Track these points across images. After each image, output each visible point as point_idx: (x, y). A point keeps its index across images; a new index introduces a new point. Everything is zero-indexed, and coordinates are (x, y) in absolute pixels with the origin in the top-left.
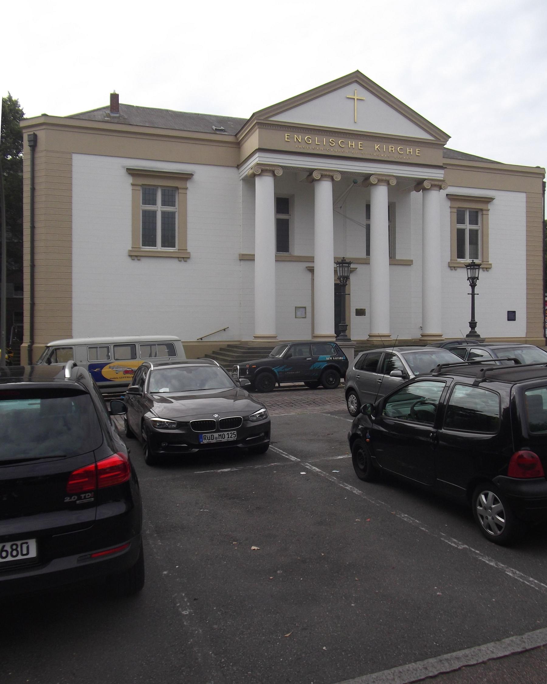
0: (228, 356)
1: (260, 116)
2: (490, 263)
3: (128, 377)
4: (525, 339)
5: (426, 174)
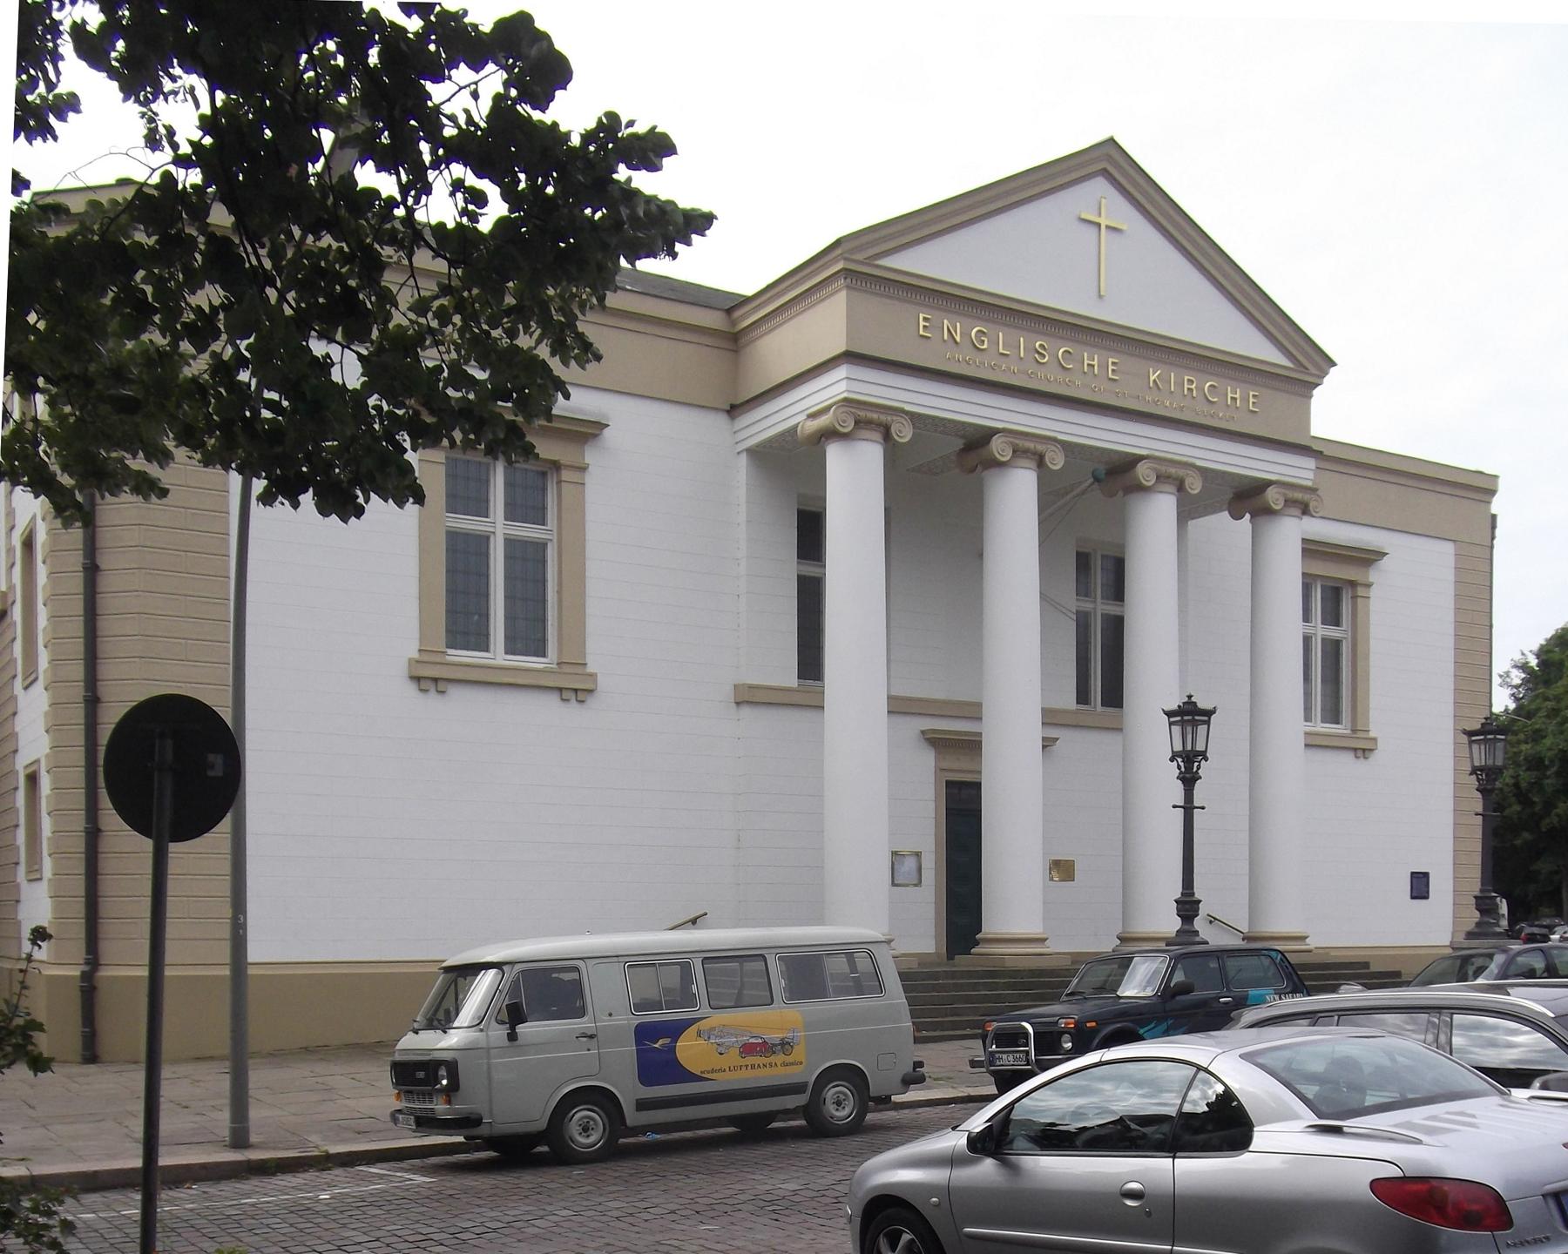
0: (986, 999)
1: (852, 251)
2: (1372, 734)
3: (753, 1067)
5: (1222, 458)
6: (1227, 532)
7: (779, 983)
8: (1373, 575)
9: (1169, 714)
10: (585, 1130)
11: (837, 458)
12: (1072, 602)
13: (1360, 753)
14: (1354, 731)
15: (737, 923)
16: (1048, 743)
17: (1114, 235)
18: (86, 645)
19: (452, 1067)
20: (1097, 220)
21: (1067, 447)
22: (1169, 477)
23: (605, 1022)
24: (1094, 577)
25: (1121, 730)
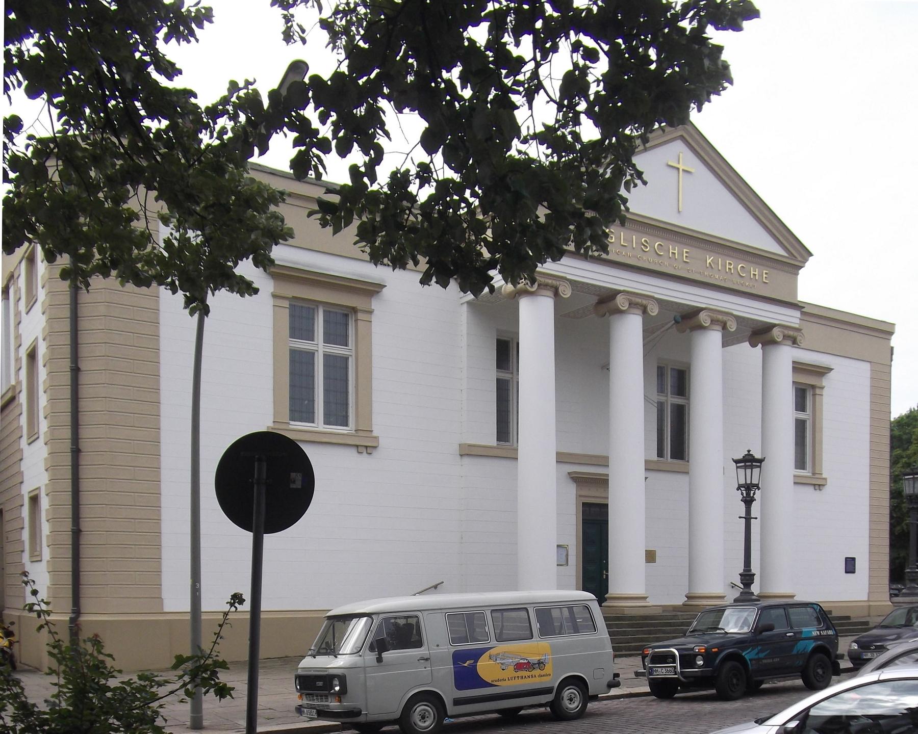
2: (824, 476)
3: (522, 677)
4: (867, 604)
6: (749, 354)
7: (536, 626)
8: (825, 382)
9: (737, 462)
10: (423, 717)
12: (655, 397)
13: (817, 487)
14: (814, 474)
15: (462, 590)
16: (646, 478)
17: (687, 176)
18: (72, 416)
19: (342, 679)
21: (660, 302)
22: (718, 321)
23: (435, 651)
24: (673, 383)
25: (687, 473)
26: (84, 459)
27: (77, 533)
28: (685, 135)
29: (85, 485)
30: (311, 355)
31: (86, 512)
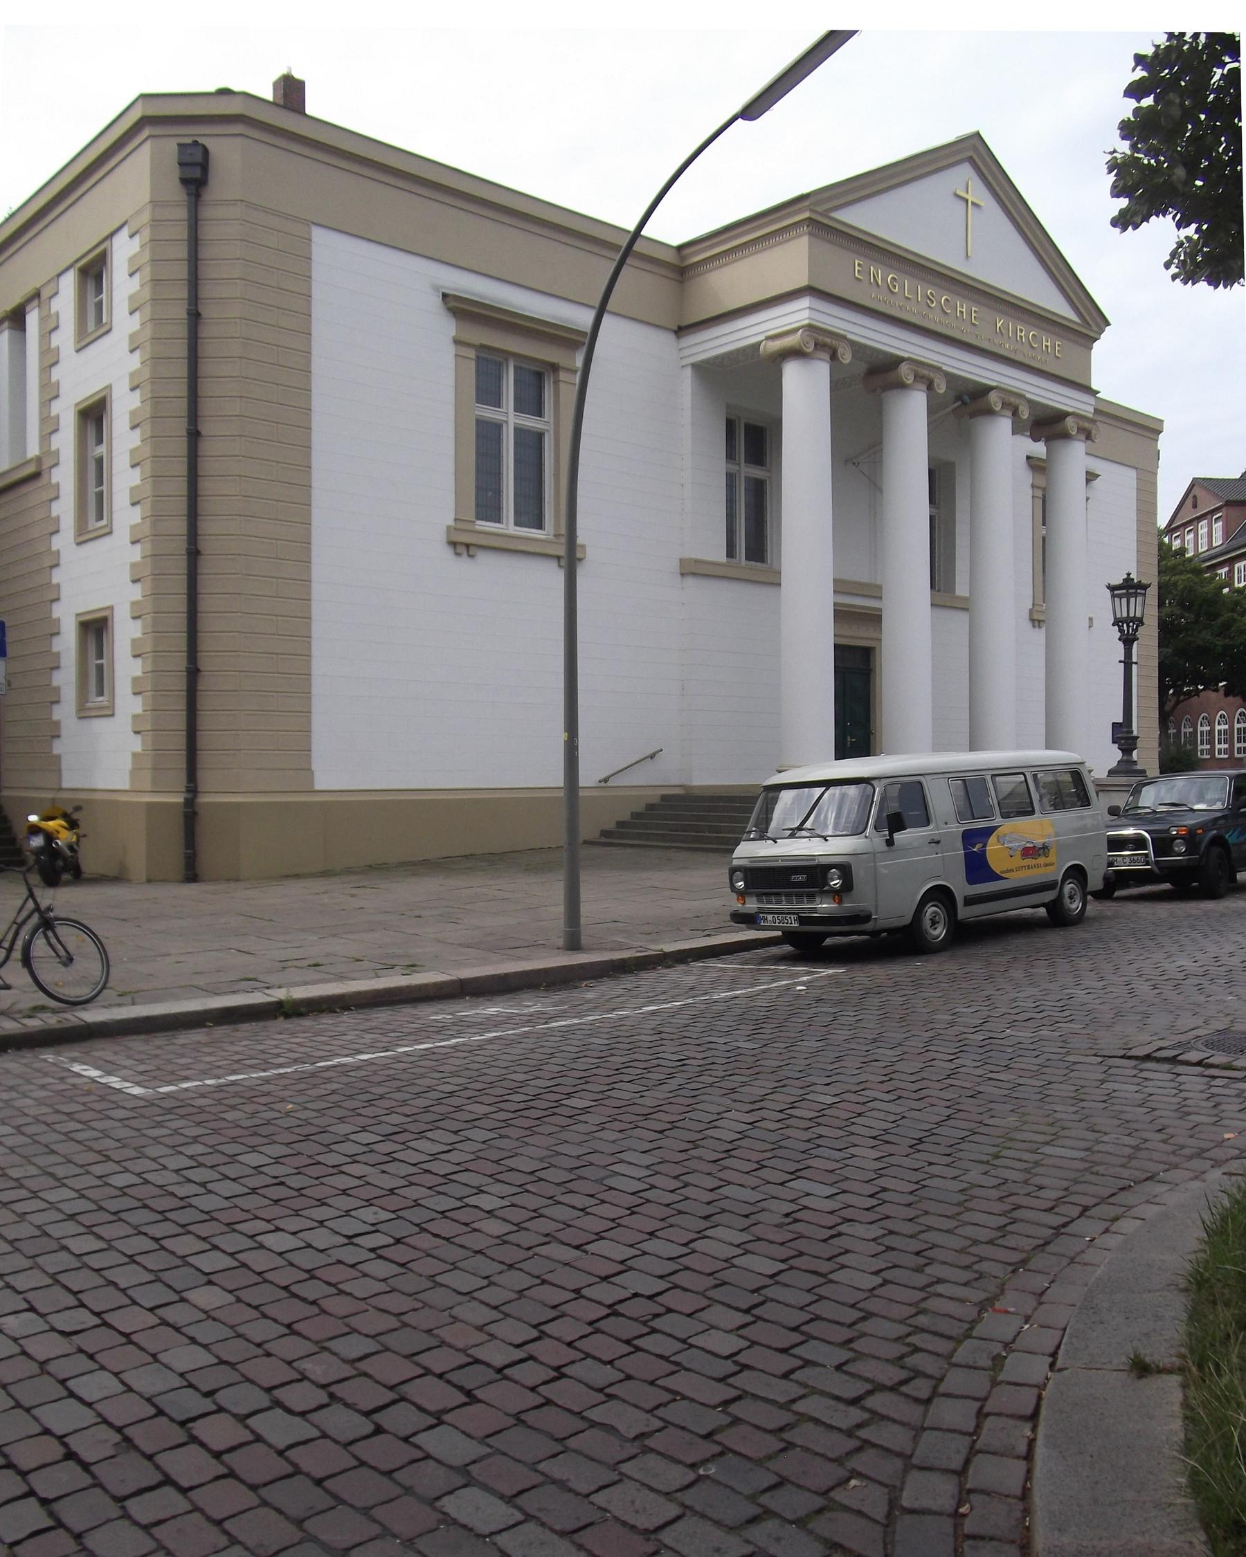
5: (1043, 393)
9: (1112, 588)
11: (792, 373)
19: (845, 870)
20: (963, 194)
25: (967, 610)
26: (207, 566)
27: (193, 673)
28: (975, 157)
29: (205, 604)
30: (498, 427)
31: (206, 644)
